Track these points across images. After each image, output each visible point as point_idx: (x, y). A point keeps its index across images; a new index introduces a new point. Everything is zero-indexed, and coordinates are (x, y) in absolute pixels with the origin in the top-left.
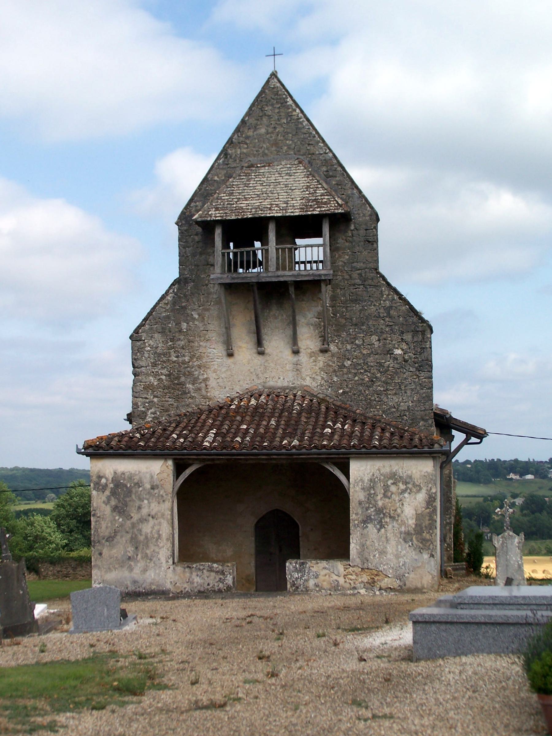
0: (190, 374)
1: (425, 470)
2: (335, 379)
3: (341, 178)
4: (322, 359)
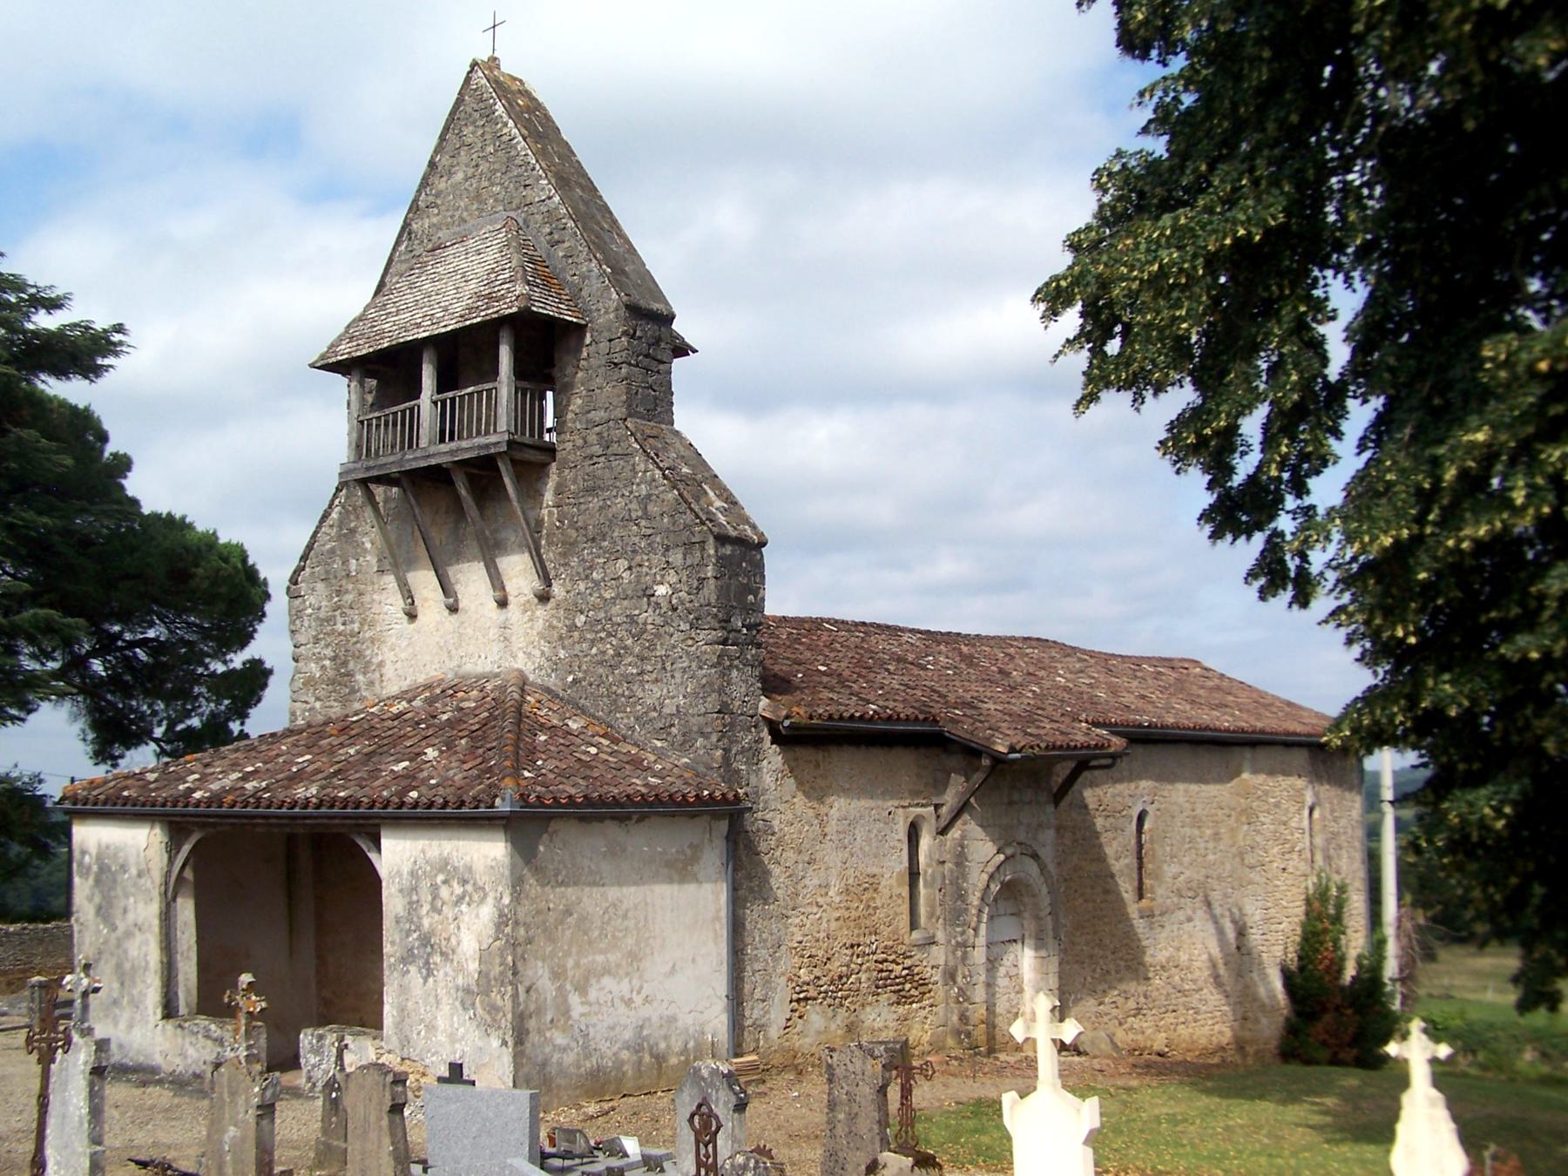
0: (359, 656)
1: (492, 855)
2: (562, 654)
3: (572, 243)
4: (541, 612)
